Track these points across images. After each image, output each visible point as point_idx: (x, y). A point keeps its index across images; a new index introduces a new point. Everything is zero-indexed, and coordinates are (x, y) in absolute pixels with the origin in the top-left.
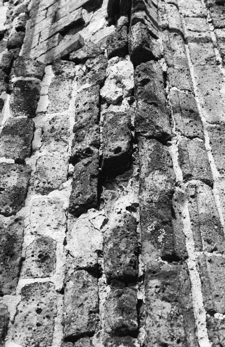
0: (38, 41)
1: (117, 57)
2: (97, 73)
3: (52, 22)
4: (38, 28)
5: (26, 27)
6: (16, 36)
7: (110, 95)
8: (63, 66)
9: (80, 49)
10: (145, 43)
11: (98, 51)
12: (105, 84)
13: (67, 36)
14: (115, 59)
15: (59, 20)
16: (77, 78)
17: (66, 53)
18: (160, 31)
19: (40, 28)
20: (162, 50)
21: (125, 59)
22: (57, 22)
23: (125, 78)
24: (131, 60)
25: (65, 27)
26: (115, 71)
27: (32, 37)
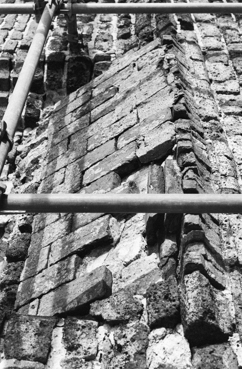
0: (46, 260)
1: (163, 329)
2: (132, 360)
3: (67, 230)
4: (49, 235)
5: (33, 225)
6: (18, 241)
8: (79, 333)
9: (107, 300)
10: (209, 312)
11: (134, 309)
13: (87, 258)
14: (160, 331)
15: (76, 229)
16: (101, 354)
17: (85, 300)
18: (226, 271)
19: (51, 234)
20: (233, 313)
21: (176, 331)
22: (74, 231)
24: (186, 336)
25: (85, 246)
26: (161, 355)
27: (40, 247)
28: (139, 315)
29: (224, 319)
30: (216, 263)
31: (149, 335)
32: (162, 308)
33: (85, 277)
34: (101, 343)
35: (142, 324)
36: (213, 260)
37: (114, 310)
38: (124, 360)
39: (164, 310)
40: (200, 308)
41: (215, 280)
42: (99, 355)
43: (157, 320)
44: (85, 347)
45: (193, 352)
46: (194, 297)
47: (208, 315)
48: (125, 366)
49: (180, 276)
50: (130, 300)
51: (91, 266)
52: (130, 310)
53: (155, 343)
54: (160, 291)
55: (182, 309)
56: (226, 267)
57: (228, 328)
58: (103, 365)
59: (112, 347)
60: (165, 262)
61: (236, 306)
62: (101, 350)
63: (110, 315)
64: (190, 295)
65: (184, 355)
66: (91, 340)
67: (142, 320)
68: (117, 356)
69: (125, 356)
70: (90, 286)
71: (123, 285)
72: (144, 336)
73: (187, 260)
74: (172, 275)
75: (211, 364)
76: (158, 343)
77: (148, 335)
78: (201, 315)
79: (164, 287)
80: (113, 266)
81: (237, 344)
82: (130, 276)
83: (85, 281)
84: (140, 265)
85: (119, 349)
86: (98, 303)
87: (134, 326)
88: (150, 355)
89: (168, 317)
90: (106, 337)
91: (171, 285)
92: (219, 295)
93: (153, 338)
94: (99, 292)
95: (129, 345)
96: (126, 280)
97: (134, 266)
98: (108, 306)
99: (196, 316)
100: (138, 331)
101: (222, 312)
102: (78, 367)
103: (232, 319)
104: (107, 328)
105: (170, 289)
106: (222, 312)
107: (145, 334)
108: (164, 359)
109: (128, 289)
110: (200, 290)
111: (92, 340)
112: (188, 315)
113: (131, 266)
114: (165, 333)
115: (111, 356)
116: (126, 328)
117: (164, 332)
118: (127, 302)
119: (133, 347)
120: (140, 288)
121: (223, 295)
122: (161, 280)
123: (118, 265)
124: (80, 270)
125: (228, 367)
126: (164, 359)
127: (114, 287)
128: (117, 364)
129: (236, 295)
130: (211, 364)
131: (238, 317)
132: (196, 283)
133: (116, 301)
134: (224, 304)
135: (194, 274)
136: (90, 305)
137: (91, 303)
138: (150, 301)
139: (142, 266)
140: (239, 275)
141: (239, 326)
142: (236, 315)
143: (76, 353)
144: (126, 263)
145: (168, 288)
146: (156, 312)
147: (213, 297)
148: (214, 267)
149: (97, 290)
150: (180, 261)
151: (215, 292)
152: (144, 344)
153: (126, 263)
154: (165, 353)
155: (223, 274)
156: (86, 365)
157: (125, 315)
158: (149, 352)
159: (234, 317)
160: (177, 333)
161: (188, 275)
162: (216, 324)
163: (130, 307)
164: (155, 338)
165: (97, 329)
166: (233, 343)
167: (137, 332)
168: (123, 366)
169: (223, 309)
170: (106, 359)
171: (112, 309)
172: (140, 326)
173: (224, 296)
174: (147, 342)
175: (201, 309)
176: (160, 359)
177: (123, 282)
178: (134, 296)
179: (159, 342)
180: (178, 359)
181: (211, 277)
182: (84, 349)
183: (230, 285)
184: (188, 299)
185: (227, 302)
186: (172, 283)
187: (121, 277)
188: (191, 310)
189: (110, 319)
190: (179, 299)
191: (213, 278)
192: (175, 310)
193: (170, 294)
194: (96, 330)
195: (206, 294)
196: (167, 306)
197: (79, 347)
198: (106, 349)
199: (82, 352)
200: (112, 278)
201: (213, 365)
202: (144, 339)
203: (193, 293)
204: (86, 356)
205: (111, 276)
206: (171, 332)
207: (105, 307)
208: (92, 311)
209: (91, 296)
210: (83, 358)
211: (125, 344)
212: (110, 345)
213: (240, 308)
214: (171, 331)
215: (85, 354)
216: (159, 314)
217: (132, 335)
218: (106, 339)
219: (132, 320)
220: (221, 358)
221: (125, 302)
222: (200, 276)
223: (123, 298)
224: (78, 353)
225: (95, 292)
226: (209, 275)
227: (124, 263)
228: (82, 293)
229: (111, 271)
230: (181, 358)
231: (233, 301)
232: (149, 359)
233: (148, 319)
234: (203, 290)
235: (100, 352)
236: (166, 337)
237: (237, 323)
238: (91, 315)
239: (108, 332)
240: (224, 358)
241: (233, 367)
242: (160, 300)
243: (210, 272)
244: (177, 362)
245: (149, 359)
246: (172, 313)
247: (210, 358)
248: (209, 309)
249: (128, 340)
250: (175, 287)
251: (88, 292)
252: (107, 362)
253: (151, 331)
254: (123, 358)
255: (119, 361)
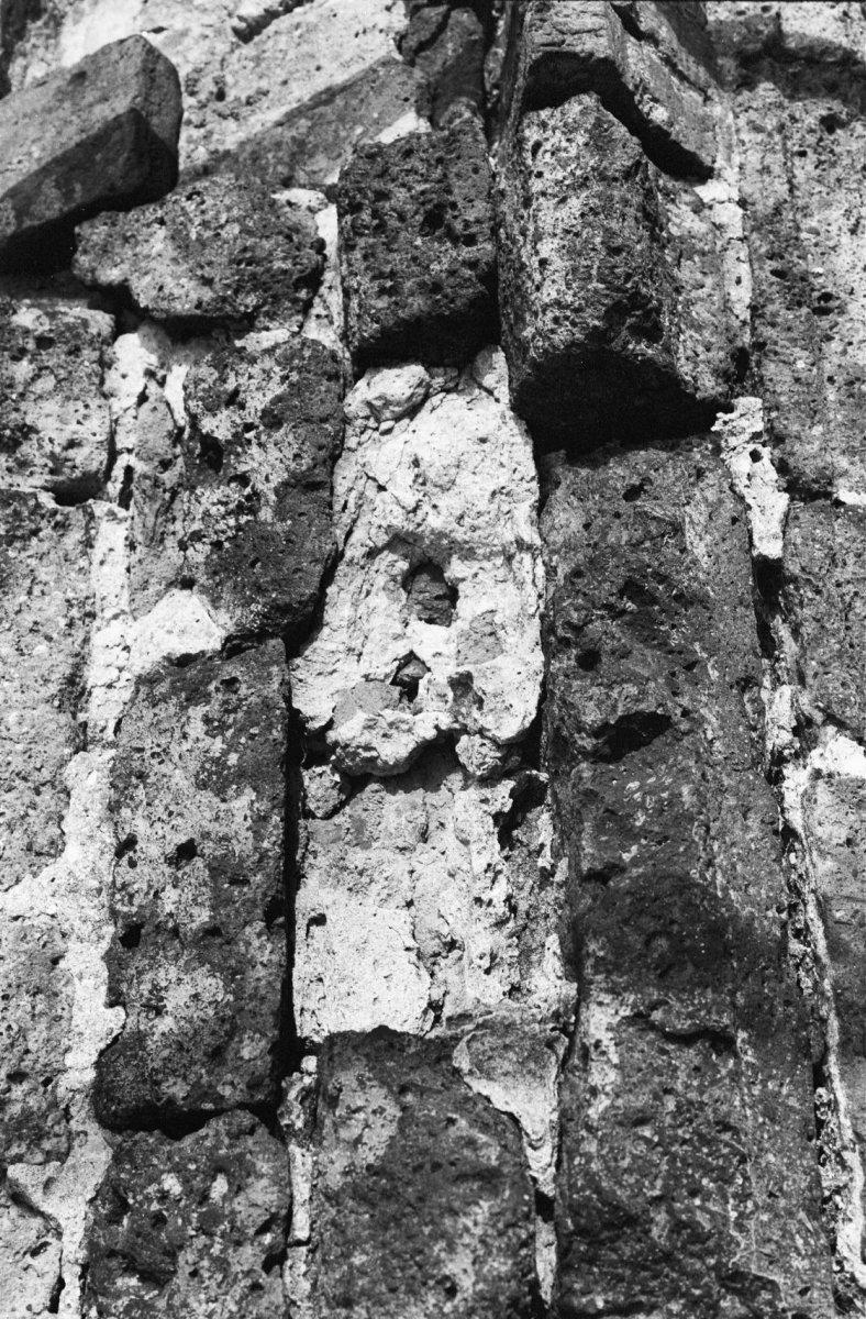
1: (414, 372)
2: (266, 514)
7: (361, 717)
8: (23, 369)
9: (152, 212)
10: (635, 307)
11: (278, 265)
12: (330, 615)
14: (397, 382)
16: (129, 470)
17: (51, 205)
18: (721, 84)
20: (742, 296)
23: (468, 554)
28: (303, 294)
29: (699, 328)
30: (675, 45)
31: (349, 399)
32: (413, 275)
33: (54, 85)
34: (127, 420)
35: (315, 342)
36: (664, 32)
37: (185, 266)
38: (228, 513)
39: (422, 285)
40: (595, 285)
41: (669, 134)
42: (118, 472)
43: (384, 331)
44: (51, 440)
45: (546, 481)
46: (567, 232)
47: (630, 321)
48: (235, 537)
49: (499, 98)
50: (262, 219)
51: (82, 27)
52: (260, 269)
53: (376, 435)
54: (403, 185)
55: (504, 275)
56: (720, 62)
57: (716, 372)
58: (137, 519)
59: (176, 436)
60: (433, 28)
61: (756, 266)
62: (130, 451)
63: (166, 291)
64: (550, 216)
65: (507, 494)
66: (80, 405)
67: (318, 316)
68: (199, 491)
69: (235, 494)
70: (72, 136)
71: (230, 136)
72: (322, 401)
73: (538, 38)
74: (464, 99)
75: (632, 557)
76: (388, 431)
77: (341, 398)
78: (596, 323)
79: (422, 168)
80: (184, 33)
81: (751, 447)
82: (266, 93)
83: (50, 111)
84: (312, 36)
85: (211, 457)
86: (114, 224)
87: (278, 351)
88: (351, 489)
89: (441, 317)
90: (153, 388)
91: (458, 158)
92: (684, 207)
93: (367, 412)
94: (116, 168)
95: (254, 441)
96: (244, 111)
97: (283, 41)
98: (158, 241)
99: (574, 324)
100: (295, 377)
101: (694, 294)
102: (19, 533)
103: (737, 323)
104: (154, 344)
105: (453, 180)
106: (694, 294)
107: (328, 391)
108: (415, 510)
109: (255, 157)
110: (599, 196)
111: (87, 406)
112: (536, 314)
113: (270, 43)
114: (421, 391)
115: (175, 480)
116: (242, 359)
117: (419, 385)
118: (246, 231)
119: (274, 453)
120: (311, 156)
121: (699, 207)
122: (409, 123)
123: (208, 32)
124: (28, 46)
125: (705, 562)
126: (415, 510)
127: (190, 141)
128: (197, 526)
129: (759, 207)
130: (632, 557)
131: (762, 316)
132: (577, 158)
133: (197, 221)
134: (703, 254)
135: (573, 108)
136: (77, 230)
137: (79, 223)
138: (357, 230)
139: (321, 44)
140: (780, 106)
141: (766, 362)
142: (754, 309)
143: (11, 463)
144: (243, 25)
145: (445, 175)
146: (382, 291)
147: (652, 220)
148: (666, 70)
149: (108, 162)
150: (501, 23)
151: (667, 195)
152: (324, 441)
153: (243, 25)
154: (421, 480)
155: (707, 99)
156: (57, 526)
157: (236, 292)
158: (345, 475)
159: (746, 315)
160: (477, 391)
161: (544, 114)
162: (662, 359)
163: (259, 253)
164: (374, 411)
165: (110, 350)
166: (733, 441)
167: (292, 385)
168: (228, 539)
169: (699, 276)
170: (149, 493)
171: (175, 260)
172: (307, 353)
173: (706, 212)
174: (337, 432)
175: (596, 291)
176: (398, 511)
177: (231, 120)
178: (282, 196)
179: (396, 431)
180: (479, 514)
181: (651, 121)
182: (48, 448)
183: (737, 159)
184: (538, 238)
185: (719, 243)
186: (465, 152)
187: (221, 96)
188: (549, 293)
189: (167, 311)
190: (497, 223)
191: (659, 127)
192: (474, 285)
193: (454, 206)
194: (102, 353)
195: (623, 216)
196: (435, 267)
197: (26, 437)
198: (150, 445)
199: (39, 461)
200: (180, 94)
201: (638, 560)
202: (324, 420)
203: (563, 213)
204: (61, 478)
205: (172, 87)
206: (451, 385)
207: (143, 249)
208: (84, 260)
209: (78, 187)
210: (46, 489)
211: (235, 435)
212: (169, 426)
213: (774, 272)
214: (452, 379)
215: (52, 472)
216: (396, 303)
217: (270, 396)
218: (152, 399)
219: (271, 316)
220: (677, 529)
221: (236, 228)
222: (598, 123)
223: (229, 209)
224: (23, 464)
225: (98, 168)
226: (640, 112)
227: (235, 22)
228: (35, 167)
229: (174, 60)
230: (494, 507)
231: (743, 239)
232: (345, 507)
233: (346, 322)
234: (611, 198)
235: (123, 460)
236: (428, 405)
237: (760, 346)
238: (82, 282)
239: (162, 366)
240: (692, 522)
241: (730, 560)
242: (403, 234)
243: (646, 97)
244: (476, 523)
245: (345, 507)
246: (458, 303)
247: (626, 525)
248: (638, 293)
249: (250, 420)
250: (476, 171)
251: (65, 168)
252: (156, 506)
253: (357, 377)
254: (225, 504)
255: (207, 514)
